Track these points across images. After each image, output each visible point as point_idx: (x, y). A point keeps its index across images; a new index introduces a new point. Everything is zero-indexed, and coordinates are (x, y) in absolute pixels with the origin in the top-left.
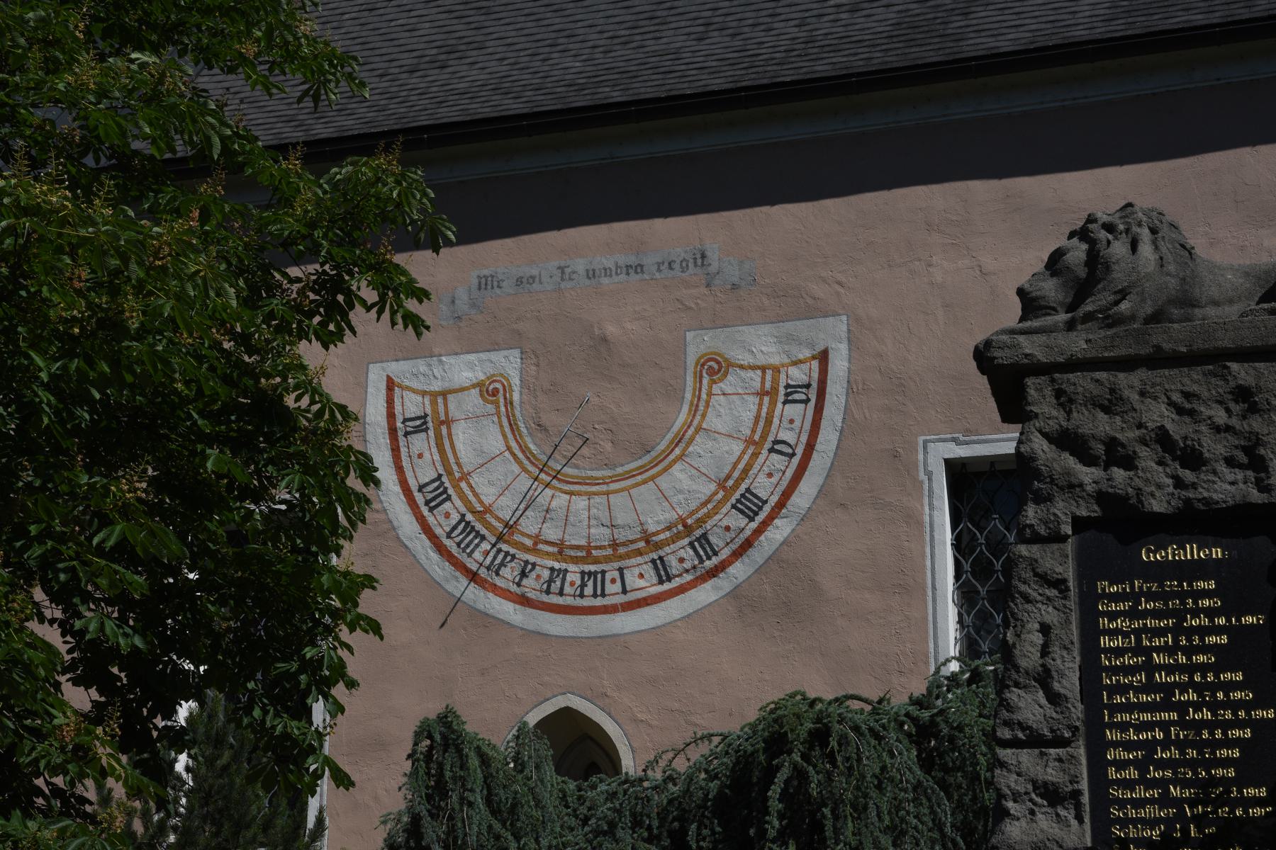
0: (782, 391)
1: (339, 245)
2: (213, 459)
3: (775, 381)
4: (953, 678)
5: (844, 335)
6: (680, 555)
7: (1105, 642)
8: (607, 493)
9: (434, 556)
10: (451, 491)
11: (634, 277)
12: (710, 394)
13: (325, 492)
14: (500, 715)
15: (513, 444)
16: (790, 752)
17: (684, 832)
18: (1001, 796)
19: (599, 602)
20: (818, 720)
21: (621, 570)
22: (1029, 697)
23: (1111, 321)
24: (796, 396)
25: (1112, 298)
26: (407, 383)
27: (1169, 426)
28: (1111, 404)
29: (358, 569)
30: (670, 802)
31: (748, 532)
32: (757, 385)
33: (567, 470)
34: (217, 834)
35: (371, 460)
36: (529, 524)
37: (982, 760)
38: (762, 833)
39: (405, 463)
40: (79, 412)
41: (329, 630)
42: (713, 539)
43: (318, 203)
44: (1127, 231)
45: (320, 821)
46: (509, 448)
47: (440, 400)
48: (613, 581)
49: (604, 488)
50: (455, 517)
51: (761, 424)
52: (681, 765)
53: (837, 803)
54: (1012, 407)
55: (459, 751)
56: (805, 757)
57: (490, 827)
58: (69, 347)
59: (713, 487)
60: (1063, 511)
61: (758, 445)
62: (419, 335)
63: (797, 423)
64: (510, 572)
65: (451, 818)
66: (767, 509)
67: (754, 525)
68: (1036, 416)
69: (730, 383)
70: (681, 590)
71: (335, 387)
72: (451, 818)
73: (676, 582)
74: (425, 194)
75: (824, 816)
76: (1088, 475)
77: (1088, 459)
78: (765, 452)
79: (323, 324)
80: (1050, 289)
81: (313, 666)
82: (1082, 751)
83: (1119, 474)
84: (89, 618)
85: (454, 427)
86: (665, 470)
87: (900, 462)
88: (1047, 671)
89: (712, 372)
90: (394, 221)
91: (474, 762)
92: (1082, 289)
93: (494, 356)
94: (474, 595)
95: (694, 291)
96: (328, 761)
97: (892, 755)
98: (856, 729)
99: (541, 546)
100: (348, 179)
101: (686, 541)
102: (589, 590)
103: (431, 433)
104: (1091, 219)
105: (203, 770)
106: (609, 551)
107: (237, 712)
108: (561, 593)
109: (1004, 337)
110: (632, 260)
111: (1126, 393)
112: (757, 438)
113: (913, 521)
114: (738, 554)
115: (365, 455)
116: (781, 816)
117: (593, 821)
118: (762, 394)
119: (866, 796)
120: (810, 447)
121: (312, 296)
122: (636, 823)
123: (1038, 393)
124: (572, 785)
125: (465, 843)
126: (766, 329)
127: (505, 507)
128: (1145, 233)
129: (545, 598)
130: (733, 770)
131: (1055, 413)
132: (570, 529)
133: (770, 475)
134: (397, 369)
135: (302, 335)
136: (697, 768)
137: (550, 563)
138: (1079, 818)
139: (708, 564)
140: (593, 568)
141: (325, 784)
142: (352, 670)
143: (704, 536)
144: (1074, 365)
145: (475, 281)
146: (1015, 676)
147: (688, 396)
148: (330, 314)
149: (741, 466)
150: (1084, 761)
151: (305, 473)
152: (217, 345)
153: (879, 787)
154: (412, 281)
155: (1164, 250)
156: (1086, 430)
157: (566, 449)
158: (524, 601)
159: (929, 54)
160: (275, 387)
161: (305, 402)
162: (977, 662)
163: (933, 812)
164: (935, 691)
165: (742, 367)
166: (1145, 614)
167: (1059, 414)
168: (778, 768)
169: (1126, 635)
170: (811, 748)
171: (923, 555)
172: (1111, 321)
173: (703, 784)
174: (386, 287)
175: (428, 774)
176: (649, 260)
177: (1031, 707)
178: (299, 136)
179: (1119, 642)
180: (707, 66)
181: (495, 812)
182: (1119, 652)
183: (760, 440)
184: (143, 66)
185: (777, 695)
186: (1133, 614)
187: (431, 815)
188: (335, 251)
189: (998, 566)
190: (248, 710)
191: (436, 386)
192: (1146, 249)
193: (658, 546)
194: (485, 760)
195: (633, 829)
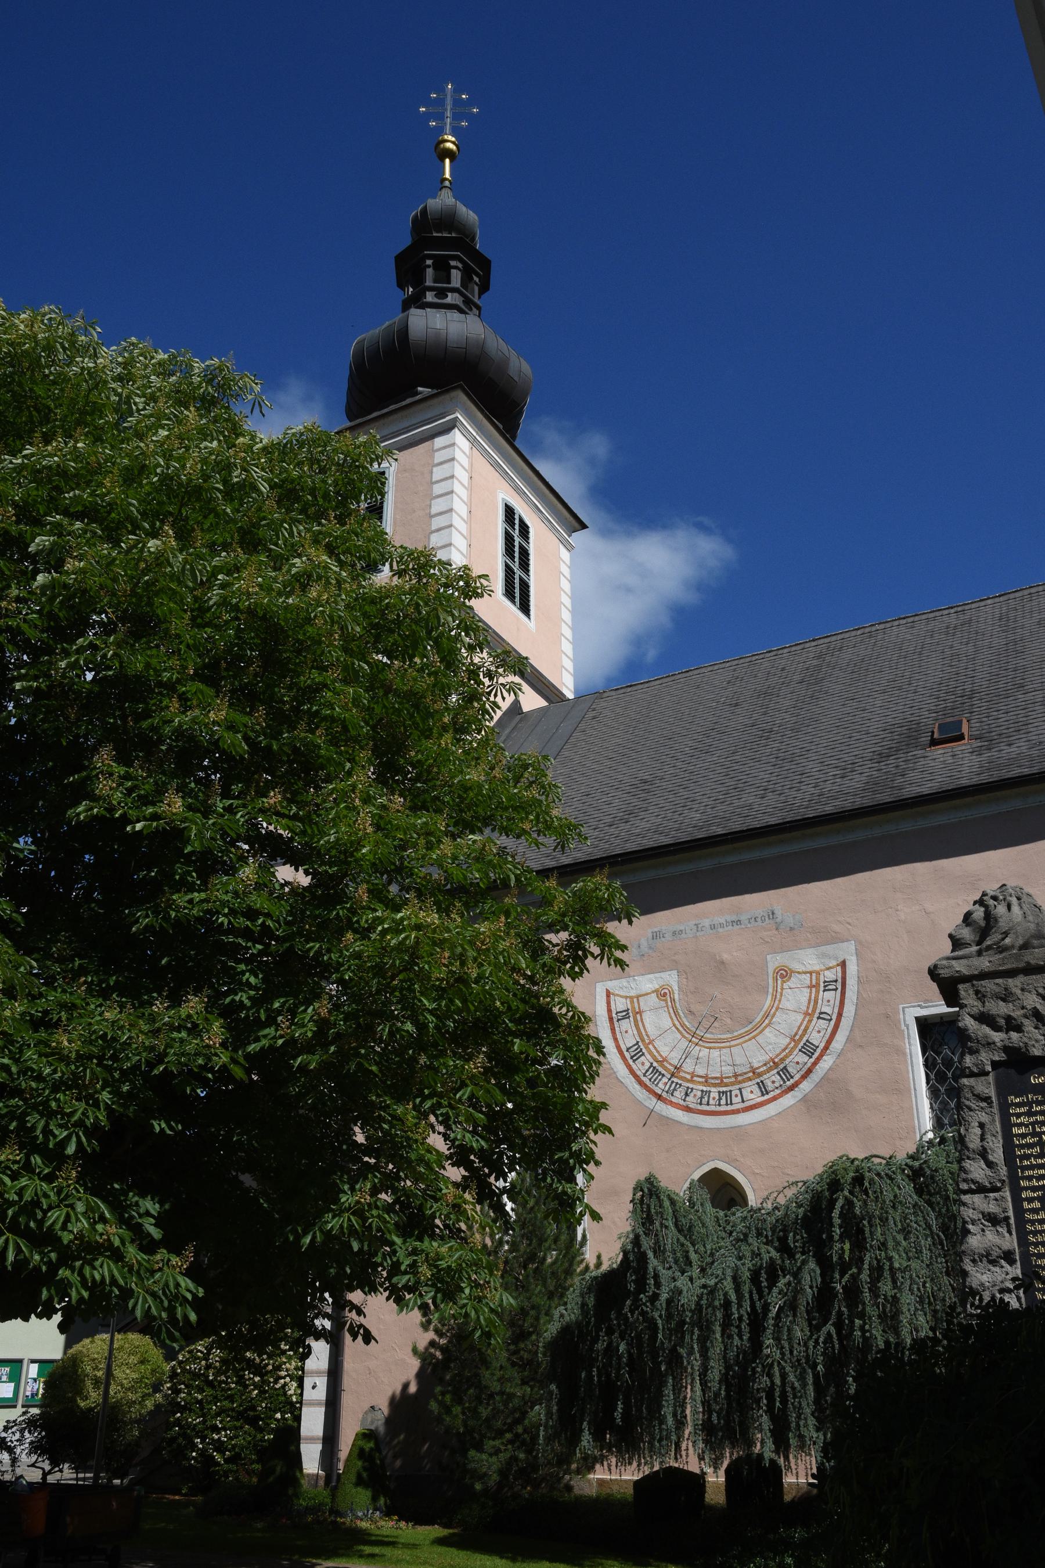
0: (822, 985)
1: (578, 925)
2: (517, 1045)
3: (818, 979)
4: (930, 1142)
5: (854, 951)
6: (772, 1079)
7: (1015, 1130)
8: (730, 1047)
9: (637, 1087)
10: (644, 1050)
11: (736, 927)
12: (782, 989)
13: (577, 1060)
14: (679, 1178)
15: (677, 1023)
16: (842, 1190)
17: (786, 1238)
18: (965, 1222)
19: (729, 1108)
20: (857, 1171)
21: (740, 1089)
22: (976, 1165)
23: (1002, 949)
24: (830, 987)
25: (1000, 937)
26: (617, 992)
27: (1039, 1007)
28: (1006, 997)
29: (598, 1099)
30: (777, 1221)
31: (809, 1065)
32: (808, 982)
33: (707, 1035)
34: (530, 1245)
35: (600, 1042)
36: (688, 1067)
37: (950, 1188)
38: (831, 1238)
39: (619, 1036)
40: (448, 1023)
41: (584, 1133)
42: (790, 1069)
43: (566, 903)
44: (1005, 899)
45: (584, 1236)
46: (674, 1025)
47: (635, 1000)
48: (736, 1096)
49: (728, 1044)
50: (647, 1065)
51: (812, 1003)
52: (782, 1200)
53: (871, 1218)
54: (950, 995)
55: (658, 1197)
56: (851, 1192)
57: (678, 1239)
58: (441, 992)
59: (788, 1040)
60: (986, 1058)
61: (811, 1015)
62: (623, 970)
63: (832, 1002)
64: (679, 1094)
65: (656, 1235)
66: (819, 1051)
67: (812, 1060)
68: (966, 1006)
69: (793, 982)
70: (774, 1099)
71: (580, 1003)
72: (656, 1235)
73: (771, 1095)
74: (622, 894)
75: (864, 1225)
76: (997, 1037)
77: (997, 1028)
78: (815, 1019)
79: (572, 968)
80: (966, 934)
81: (576, 1155)
82: (1008, 1194)
83: (1014, 1035)
84: (458, 1133)
85: (644, 1015)
86: (761, 1032)
87: (891, 1020)
88: (984, 1149)
89: (782, 976)
90: (606, 910)
91: (667, 1203)
92: (984, 933)
93: (662, 975)
94: (661, 1107)
95: (769, 933)
96: (587, 1206)
97: (900, 1189)
98: (878, 1175)
99: (695, 1078)
100: (581, 890)
101: (775, 1071)
102: (723, 1102)
103: (631, 1019)
104: (984, 894)
105: (521, 1210)
106: (733, 1079)
107: (537, 1181)
108: (708, 1104)
109: (944, 962)
110: (734, 918)
111: (1014, 990)
112: (810, 1011)
113: (900, 1052)
114: (804, 1077)
115: (597, 1038)
116: (840, 1227)
117: (734, 1234)
118: (811, 987)
119: (887, 1212)
120: (840, 1015)
121: (565, 953)
122: (759, 1234)
123: (964, 991)
124: (722, 1213)
125: (665, 1249)
126: (810, 951)
127: (674, 1058)
128: (1014, 900)
129: (699, 1107)
130: (811, 1202)
131: (976, 1003)
132: (710, 1068)
133: (819, 1032)
134: (611, 985)
135: (561, 973)
136: (790, 1201)
137: (701, 1088)
138: (1010, 1232)
139: (788, 1083)
140: (724, 1089)
141: (587, 1218)
142: (598, 1156)
143: (785, 1068)
144: (983, 976)
145: (650, 935)
146: (967, 1153)
147: (771, 990)
148: (575, 960)
149: (803, 1028)
150: (1009, 1199)
151: (566, 1050)
152: (517, 983)
153: (894, 1207)
154: (617, 941)
155: (1025, 908)
156: (994, 1012)
157: (706, 1024)
158: (688, 1109)
159: (885, 797)
160: (548, 1003)
161: (564, 1011)
162: (943, 1132)
163: (925, 1219)
164: (921, 1150)
165: (799, 973)
166: (1036, 1113)
167: (980, 1004)
168: (836, 1200)
169: (1026, 1126)
170: (854, 1187)
171: (908, 1072)
172: (1002, 949)
173: (794, 1210)
174: (604, 945)
175: (642, 1211)
176: (744, 918)
177: (977, 1170)
178: (553, 864)
179: (1023, 1130)
180: (767, 812)
181: (680, 1231)
182: (1023, 1136)
183: (812, 1013)
184: (474, 842)
185: (833, 1157)
186: (1030, 1114)
187: (645, 1234)
188: (576, 928)
189: (950, 1075)
190: (544, 1179)
191: (633, 993)
192: (1015, 908)
193: (760, 1075)
194: (673, 1202)
195: (757, 1237)
